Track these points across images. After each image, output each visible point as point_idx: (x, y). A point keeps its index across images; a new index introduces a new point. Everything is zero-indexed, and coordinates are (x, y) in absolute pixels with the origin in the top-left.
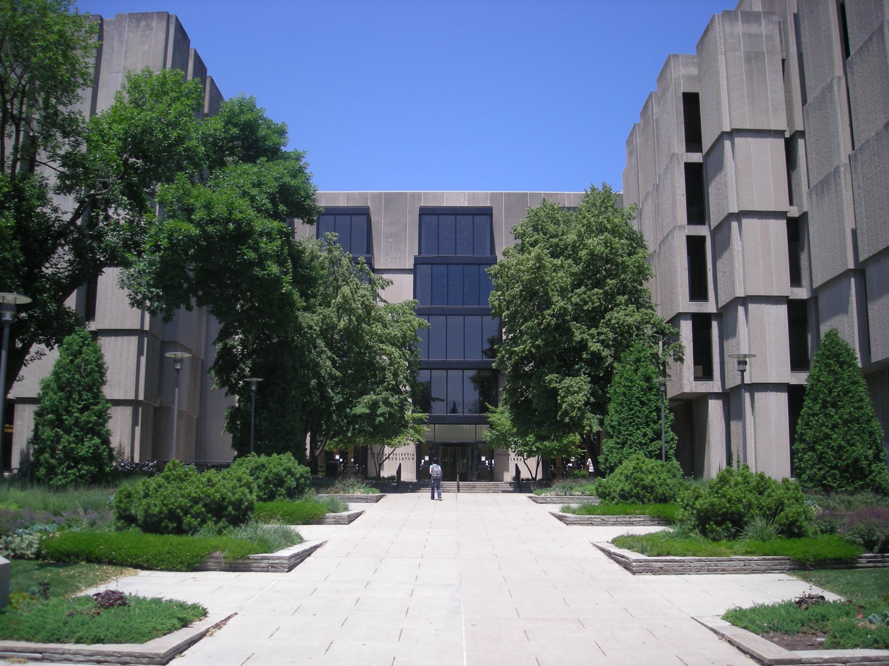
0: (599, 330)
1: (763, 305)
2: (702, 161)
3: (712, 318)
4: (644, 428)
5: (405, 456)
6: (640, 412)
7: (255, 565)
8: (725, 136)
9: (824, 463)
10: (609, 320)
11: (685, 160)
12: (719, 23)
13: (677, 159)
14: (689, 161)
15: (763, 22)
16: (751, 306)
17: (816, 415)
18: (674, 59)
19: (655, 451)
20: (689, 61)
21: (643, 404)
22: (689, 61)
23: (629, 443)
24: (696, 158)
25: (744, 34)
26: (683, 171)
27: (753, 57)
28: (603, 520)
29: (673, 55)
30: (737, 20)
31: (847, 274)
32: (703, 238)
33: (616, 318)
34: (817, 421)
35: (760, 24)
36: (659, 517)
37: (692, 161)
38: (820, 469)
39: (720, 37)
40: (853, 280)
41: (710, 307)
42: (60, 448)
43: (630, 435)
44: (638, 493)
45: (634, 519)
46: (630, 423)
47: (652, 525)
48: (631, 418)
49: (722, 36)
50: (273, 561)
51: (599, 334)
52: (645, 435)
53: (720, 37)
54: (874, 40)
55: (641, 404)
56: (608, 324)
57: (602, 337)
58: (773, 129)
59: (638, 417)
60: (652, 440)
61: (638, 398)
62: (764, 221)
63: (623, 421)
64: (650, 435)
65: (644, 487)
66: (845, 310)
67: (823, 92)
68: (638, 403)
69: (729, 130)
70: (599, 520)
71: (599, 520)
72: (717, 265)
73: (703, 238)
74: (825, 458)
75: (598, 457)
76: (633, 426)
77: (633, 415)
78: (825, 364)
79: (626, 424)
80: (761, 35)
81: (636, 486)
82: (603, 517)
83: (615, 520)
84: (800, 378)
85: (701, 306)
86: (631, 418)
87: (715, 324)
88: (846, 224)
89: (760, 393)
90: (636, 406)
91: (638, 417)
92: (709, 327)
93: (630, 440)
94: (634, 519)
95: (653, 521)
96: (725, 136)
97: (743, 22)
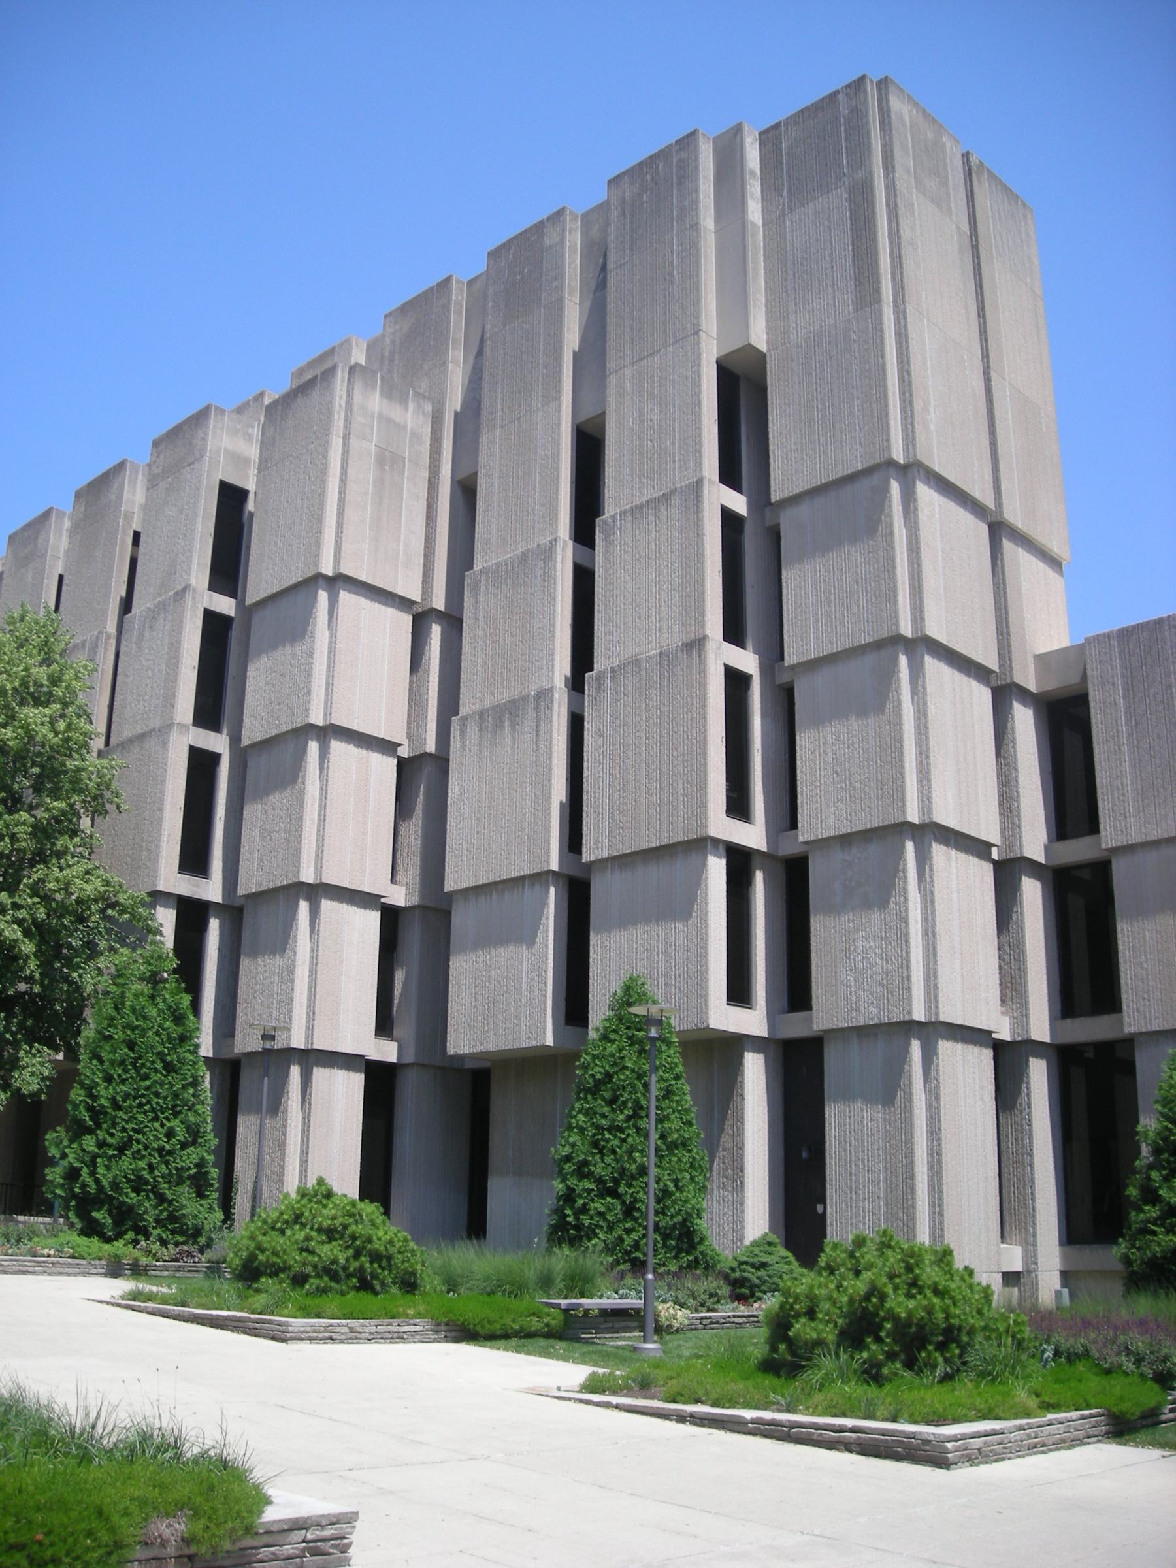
0: (17, 899)
1: (344, 905)
2: (232, 614)
3: (211, 912)
4: (168, 1119)
5: (1136, 1222)
6: (162, 1084)
7: (265, 1552)
8: (321, 582)
9: (635, 1219)
10: (42, 881)
11: (206, 605)
12: (342, 381)
13: (194, 598)
14: (213, 609)
15: (411, 406)
16: (326, 905)
17: (620, 1129)
18: (216, 415)
19: (189, 1168)
20: (239, 427)
21: (169, 1068)
22: (239, 427)
23: (135, 1147)
24: (225, 605)
25: (380, 416)
26: (199, 622)
27: (388, 461)
28: (352, 1330)
29: (217, 408)
30: (374, 387)
31: (541, 878)
32: (215, 758)
33: (57, 880)
34: (624, 1141)
35: (406, 409)
36: (447, 1324)
37: (218, 610)
38: (628, 1231)
39: (340, 406)
40: (552, 890)
41: (211, 890)
42: (666, 1125)
43: (137, 1131)
44: (361, 1269)
45: (405, 1329)
46: (141, 1105)
47: (434, 1341)
48: (143, 1096)
49: (343, 404)
50: (320, 1534)
51: (16, 906)
52: (170, 1134)
53: (340, 406)
54: (676, 501)
55: (165, 1068)
56: (35, 890)
57: (22, 914)
58: (400, 593)
59: (157, 1095)
60: (184, 1146)
61: (161, 1055)
62: (364, 752)
63: (124, 1101)
64: (181, 1134)
65: (376, 1257)
66: (528, 937)
67: (524, 557)
68: (159, 1066)
69: (330, 574)
70: (345, 1330)
71: (345, 1330)
72: (247, 812)
73: (215, 758)
74: (639, 1210)
75: (47, 1171)
76: (145, 1113)
77: (148, 1088)
78: (629, 1038)
79: (131, 1107)
80: (405, 428)
81: (357, 1255)
82: (352, 1323)
83: (373, 1329)
84: (387, 1052)
85: (197, 886)
86: (143, 1096)
87: (214, 925)
88: (554, 792)
89: (321, 1070)
90: (156, 1071)
91: (157, 1095)
92: (203, 928)
93: (138, 1142)
94: (405, 1329)
95: (437, 1332)
96: (321, 582)
97: (382, 395)
